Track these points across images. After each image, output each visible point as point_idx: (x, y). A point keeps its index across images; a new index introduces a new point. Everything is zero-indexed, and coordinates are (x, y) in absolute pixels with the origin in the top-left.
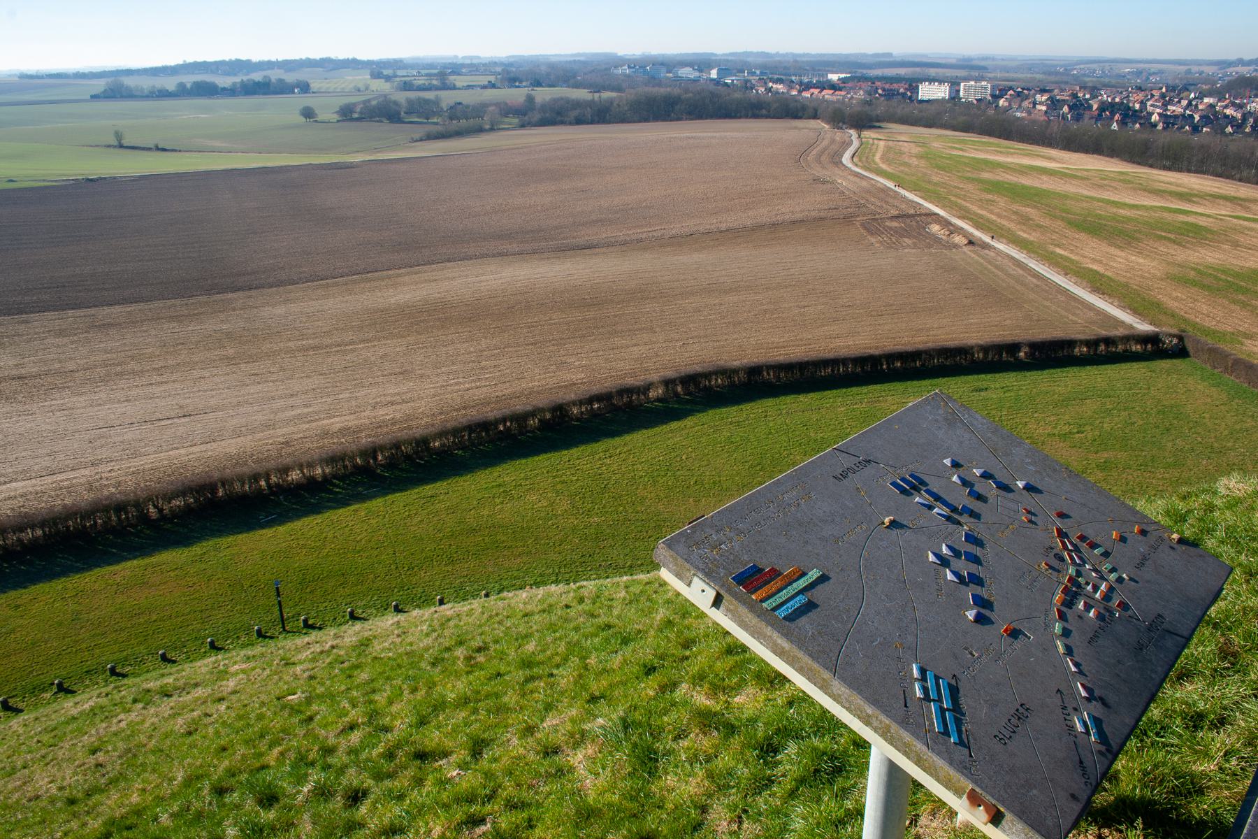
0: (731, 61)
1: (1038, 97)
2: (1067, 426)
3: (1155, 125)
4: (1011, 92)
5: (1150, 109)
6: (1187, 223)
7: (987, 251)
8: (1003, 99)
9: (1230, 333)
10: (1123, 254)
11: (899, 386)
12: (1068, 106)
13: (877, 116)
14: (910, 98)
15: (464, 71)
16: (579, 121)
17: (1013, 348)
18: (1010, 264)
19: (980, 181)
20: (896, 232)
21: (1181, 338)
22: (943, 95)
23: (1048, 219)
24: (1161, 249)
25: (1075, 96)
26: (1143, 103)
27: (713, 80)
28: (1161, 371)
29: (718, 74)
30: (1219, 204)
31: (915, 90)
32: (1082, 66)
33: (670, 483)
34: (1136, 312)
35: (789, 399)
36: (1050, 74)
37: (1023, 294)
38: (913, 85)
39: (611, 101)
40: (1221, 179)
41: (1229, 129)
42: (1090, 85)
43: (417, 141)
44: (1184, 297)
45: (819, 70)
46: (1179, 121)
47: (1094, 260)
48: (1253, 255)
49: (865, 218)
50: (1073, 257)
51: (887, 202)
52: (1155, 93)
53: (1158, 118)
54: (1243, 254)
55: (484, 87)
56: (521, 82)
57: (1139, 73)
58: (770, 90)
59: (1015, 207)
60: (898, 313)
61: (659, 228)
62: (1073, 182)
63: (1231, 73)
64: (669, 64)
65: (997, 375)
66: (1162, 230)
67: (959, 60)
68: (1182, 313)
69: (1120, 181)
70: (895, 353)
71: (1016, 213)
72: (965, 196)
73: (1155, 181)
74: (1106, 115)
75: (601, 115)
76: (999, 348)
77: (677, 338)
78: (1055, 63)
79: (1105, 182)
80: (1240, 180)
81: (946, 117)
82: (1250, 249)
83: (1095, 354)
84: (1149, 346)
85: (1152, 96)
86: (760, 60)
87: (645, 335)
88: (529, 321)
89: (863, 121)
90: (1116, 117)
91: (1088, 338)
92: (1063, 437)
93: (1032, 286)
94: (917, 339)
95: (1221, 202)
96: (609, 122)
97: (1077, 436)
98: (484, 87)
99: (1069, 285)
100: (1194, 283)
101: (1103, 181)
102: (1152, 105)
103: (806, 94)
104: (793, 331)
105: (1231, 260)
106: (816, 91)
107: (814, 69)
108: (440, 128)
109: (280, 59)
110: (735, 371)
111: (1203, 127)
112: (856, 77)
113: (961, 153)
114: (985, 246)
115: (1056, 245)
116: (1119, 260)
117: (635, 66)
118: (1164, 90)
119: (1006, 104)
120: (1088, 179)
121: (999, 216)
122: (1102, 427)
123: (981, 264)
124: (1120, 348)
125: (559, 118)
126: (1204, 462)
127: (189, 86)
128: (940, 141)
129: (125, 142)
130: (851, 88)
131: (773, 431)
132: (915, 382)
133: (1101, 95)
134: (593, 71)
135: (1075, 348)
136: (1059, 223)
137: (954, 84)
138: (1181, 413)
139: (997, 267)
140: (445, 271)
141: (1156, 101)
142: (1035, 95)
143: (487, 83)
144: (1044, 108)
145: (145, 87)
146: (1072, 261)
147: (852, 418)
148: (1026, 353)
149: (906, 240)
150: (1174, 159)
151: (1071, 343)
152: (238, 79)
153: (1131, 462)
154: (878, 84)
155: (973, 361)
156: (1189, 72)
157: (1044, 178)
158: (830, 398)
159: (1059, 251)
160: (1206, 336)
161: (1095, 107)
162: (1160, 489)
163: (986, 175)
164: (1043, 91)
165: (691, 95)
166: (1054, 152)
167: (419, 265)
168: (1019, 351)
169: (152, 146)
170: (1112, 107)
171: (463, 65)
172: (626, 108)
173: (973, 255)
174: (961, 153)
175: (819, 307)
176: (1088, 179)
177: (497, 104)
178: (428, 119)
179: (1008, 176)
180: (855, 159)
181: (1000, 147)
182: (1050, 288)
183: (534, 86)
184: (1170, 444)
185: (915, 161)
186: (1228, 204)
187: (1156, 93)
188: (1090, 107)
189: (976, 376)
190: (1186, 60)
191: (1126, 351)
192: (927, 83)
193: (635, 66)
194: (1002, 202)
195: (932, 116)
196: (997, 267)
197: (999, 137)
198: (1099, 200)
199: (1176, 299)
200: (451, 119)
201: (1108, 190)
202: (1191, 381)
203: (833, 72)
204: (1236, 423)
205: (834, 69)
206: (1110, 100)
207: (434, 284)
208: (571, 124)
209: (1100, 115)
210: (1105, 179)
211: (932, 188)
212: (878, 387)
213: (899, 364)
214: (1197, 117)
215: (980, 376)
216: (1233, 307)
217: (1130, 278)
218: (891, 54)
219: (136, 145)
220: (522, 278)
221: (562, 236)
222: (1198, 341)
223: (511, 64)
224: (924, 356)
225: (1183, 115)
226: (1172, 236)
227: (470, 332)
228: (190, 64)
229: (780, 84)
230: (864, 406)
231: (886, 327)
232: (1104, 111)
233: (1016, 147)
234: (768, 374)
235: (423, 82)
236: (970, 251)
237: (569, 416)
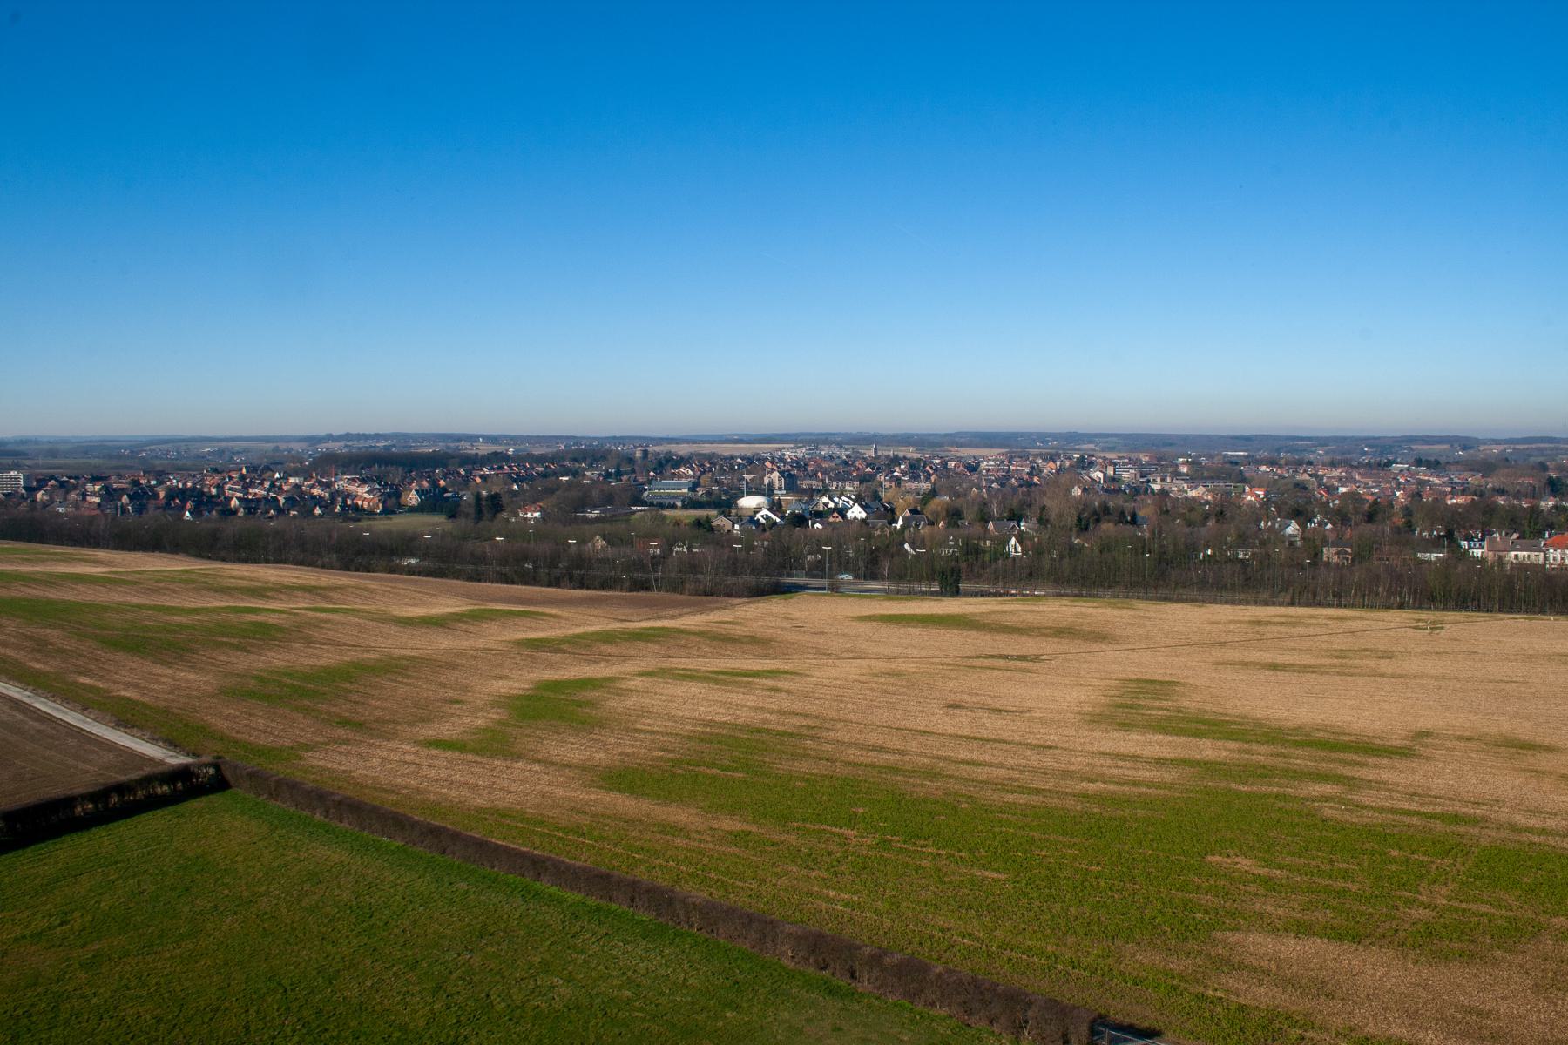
1: (89, 486)
4: (53, 482)
10: (170, 672)
12: (129, 495)
21: (217, 767)
24: (221, 658)
25: (136, 483)
26: (220, 487)
30: (297, 597)
32: (153, 447)
36: (110, 457)
41: (318, 511)
42: (158, 469)
44: (237, 713)
46: (262, 505)
47: (128, 685)
48: (328, 651)
53: (237, 503)
54: (316, 651)
57: (220, 453)
59: (31, 630)
66: (223, 635)
68: (234, 734)
69: (181, 581)
71: (31, 638)
74: (175, 503)
79: (162, 585)
80: (323, 567)
82: (324, 644)
85: (231, 478)
91: (91, 790)
93: (32, 732)
95: (299, 594)
99: (85, 722)
100: (252, 694)
101: (159, 584)
102: (231, 489)
111: (289, 510)
118: (244, 471)
120: (140, 583)
122: (98, 908)
126: (228, 921)
133: (170, 480)
135: (75, 807)
138: (208, 863)
141: (235, 483)
144: (97, 500)
146: (98, 689)
150: (248, 549)
151: (69, 802)
153: (131, 947)
156: (276, 449)
157: (80, 587)
159: (83, 680)
161: (162, 495)
164: (95, 479)
166: (101, 554)
170: (183, 494)
176: (140, 583)
179: (30, 591)
181: (28, 554)
184: (187, 908)
186: (307, 595)
187: (235, 475)
188: (156, 495)
190: (274, 437)
191: (148, 796)
197: (29, 541)
199: (228, 718)
201: (165, 594)
204: (275, 859)
206: (180, 485)
209: (168, 504)
214: (282, 500)
217: (173, 701)
225: (266, 498)
226: (235, 641)
233: (52, 551)
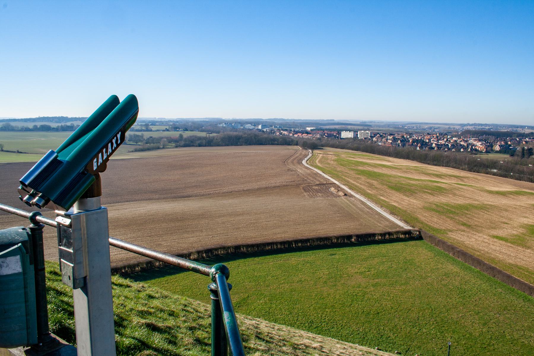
0: (268, 122)
1: (389, 137)
2: (364, 268)
3: (434, 148)
4: (378, 135)
5: (432, 142)
6: (437, 186)
7: (351, 198)
8: (375, 138)
9: (443, 230)
10: (408, 199)
11: (298, 253)
12: (400, 141)
13: (322, 144)
14: (338, 137)
15: (157, 124)
16: (200, 145)
17: (349, 237)
18: (359, 203)
19: (357, 170)
20: (316, 191)
21: (420, 232)
22: (351, 136)
23: (380, 185)
24: (425, 196)
25: (403, 137)
26: (429, 140)
27: (259, 129)
28: (410, 245)
29: (262, 127)
30: (452, 179)
31: (339, 134)
32: (409, 125)
33: (189, 294)
34: (406, 222)
35: (250, 259)
36: (395, 128)
37: (361, 215)
38: (339, 132)
39: (214, 137)
40: (455, 169)
41: (462, 150)
42: (411, 132)
43: (131, 152)
44: (428, 216)
45: (303, 126)
47: (395, 201)
48: (460, 199)
49: (305, 185)
50: (387, 200)
51: (316, 179)
52: (434, 136)
53: (435, 145)
55: (164, 131)
56: (179, 129)
57: (431, 128)
58: (281, 134)
59: (368, 180)
60: (306, 224)
61: (219, 189)
62: (395, 170)
63: (465, 129)
64: (242, 123)
65: (341, 249)
66: (426, 189)
67: (361, 122)
68: (426, 222)
69: (414, 170)
70: (298, 240)
71: (368, 183)
72: (349, 176)
73: (428, 170)
75: (209, 143)
76: (343, 237)
77: (211, 234)
79: (408, 170)
80: (462, 170)
81: (349, 145)
82: (460, 196)
83: (384, 239)
84: (407, 236)
85: (433, 137)
86: (280, 122)
87: (198, 233)
88: (151, 227)
89: (314, 146)
90: (419, 145)
91: (381, 232)
92: (361, 273)
93: (366, 212)
94: (311, 234)
95: (453, 178)
96: (212, 146)
97: (367, 273)
98: (164, 131)
100: (433, 210)
101: (408, 170)
102: (433, 140)
103: (296, 136)
104: (260, 231)
105: (452, 201)
106: (300, 134)
107: (301, 126)
108: (141, 147)
109: (80, 117)
110: (229, 248)
111: (452, 149)
112: (318, 129)
113: (353, 159)
114: (351, 196)
115: (381, 196)
116: (406, 201)
117: (228, 123)
118: (438, 135)
119: (376, 140)
121: (361, 184)
123: (348, 204)
124: (395, 236)
125: (192, 144)
127: (38, 127)
128: (345, 154)
129: (4, 149)
130: (314, 133)
131: (239, 272)
132: (305, 252)
134: (210, 125)
135: (376, 237)
136: (385, 186)
137: (355, 132)
139: (354, 205)
140: (124, 206)
141: (434, 139)
142: (387, 136)
143: (165, 129)
144: (391, 141)
145: (19, 126)
147: (275, 267)
148: (355, 239)
149: (319, 194)
150: (437, 161)
151: (374, 235)
152: (60, 125)
154: (326, 131)
155: (332, 243)
156: (449, 128)
157: (384, 169)
158: (268, 259)
159: (382, 198)
160: (434, 231)
161: (411, 141)
162: (396, 294)
163: (360, 168)
164: (391, 135)
165: (246, 135)
166: (391, 159)
167: (114, 203)
168: (352, 238)
169: (16, 151)
170: (417, 141)
171: (157, 122)
172: (220, 140)
173: (345, 200)
174: (353, 159)
175: (275, 221)
177: (167, 138)
178: (137, 143)
180: (307, 162)
182: (373, 213)
183: (184, 131)
185: (332, 162)
186: (456, 179)
187: (435, 136)
188: (409, 141)
189: (332, 249)
192: (344, 131)
193: (228, 123)
194: (363, 178)
195: (344, 145)
196: (354, 205)
197: (370, 153)
198: (403, 177)
199: (425, 216)
200: (147, 143)
201: (409, 174)
202: (421, 249)
203: (309, 127)
204: (435, 266)
205: (310, 126)
207: (117, 211)
208: (196, 146)
209: (412, 144)
210: (408, 169)
211: (336, 173)
212: (289, 254)
213: (300, 245)
214: (450, 145)
215: (334, 249)
216: (447, 219)
217: (408, 208)
218: (334, 120)
219: (9, 150)
220: (155, 209)
221: (178, 192)
222: (426, 233)
223: (177, 122)
224: (310, 241)
227: (125, 231)
228: (41, 117)
229: (286, 131)
230: (281, 262)
231: (300, 229)
232: (414, 143)
233: (376, 156)
234: (243, 249)
235: (138, 128)
236: (344, 198)
237: (154, 266)
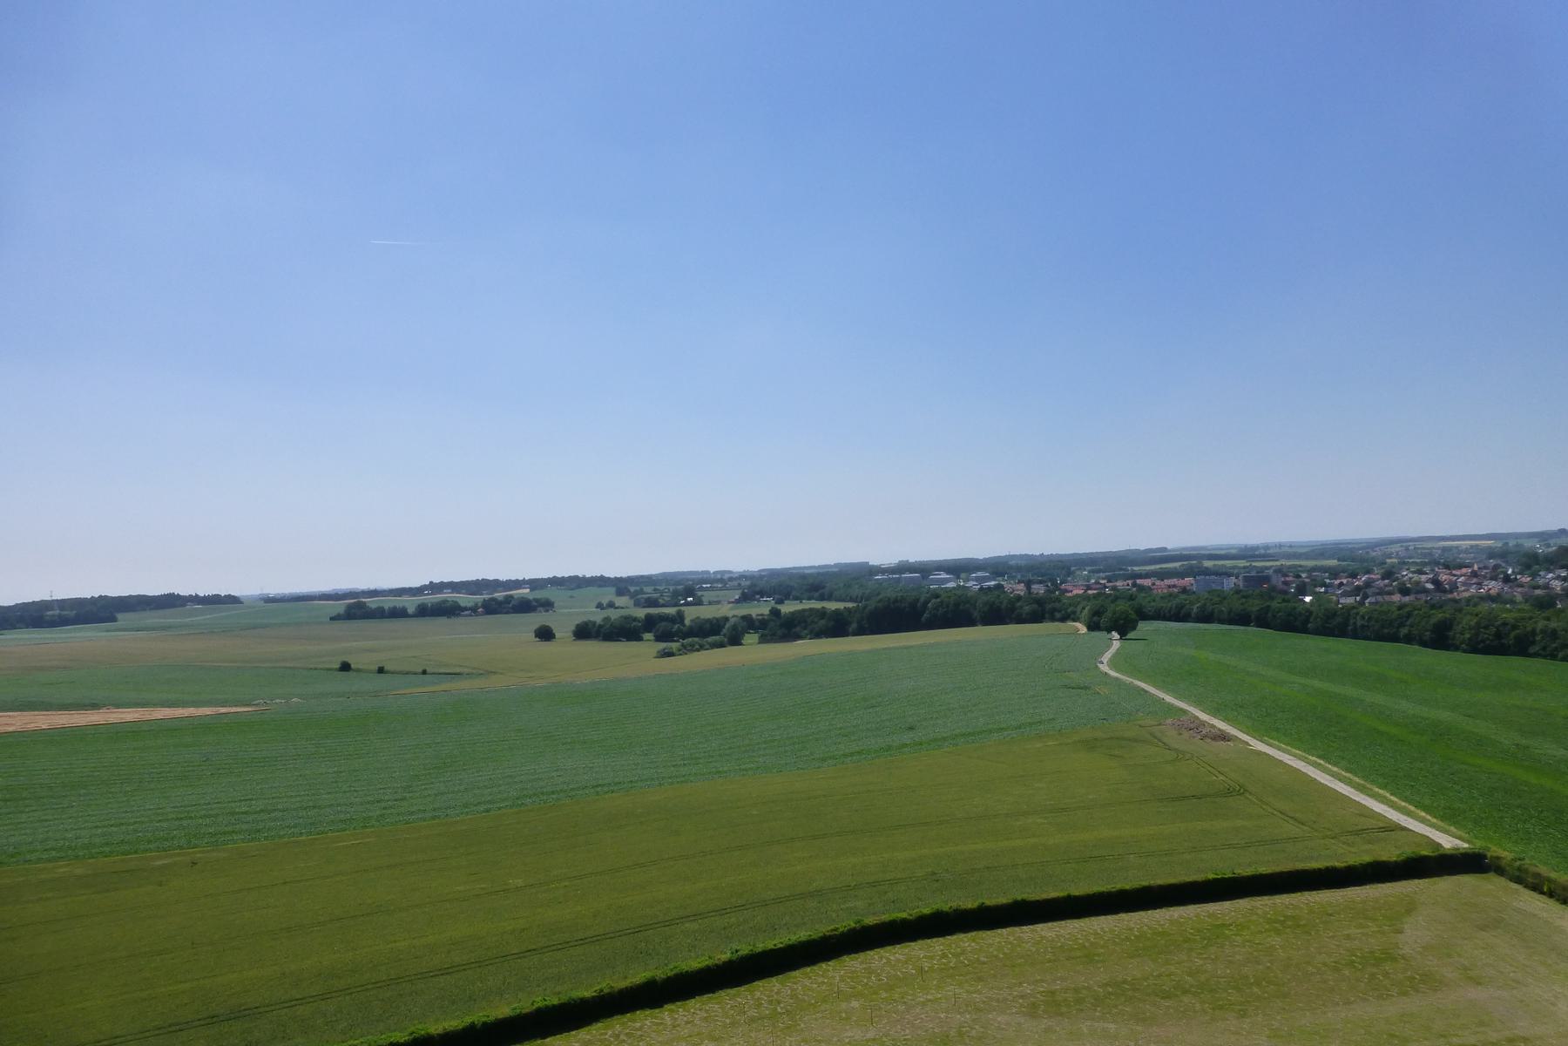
73: (69, 865)
78: (1356, 546)
109: (526, 578)
143: (120, 616)
218: (1166, 548)
